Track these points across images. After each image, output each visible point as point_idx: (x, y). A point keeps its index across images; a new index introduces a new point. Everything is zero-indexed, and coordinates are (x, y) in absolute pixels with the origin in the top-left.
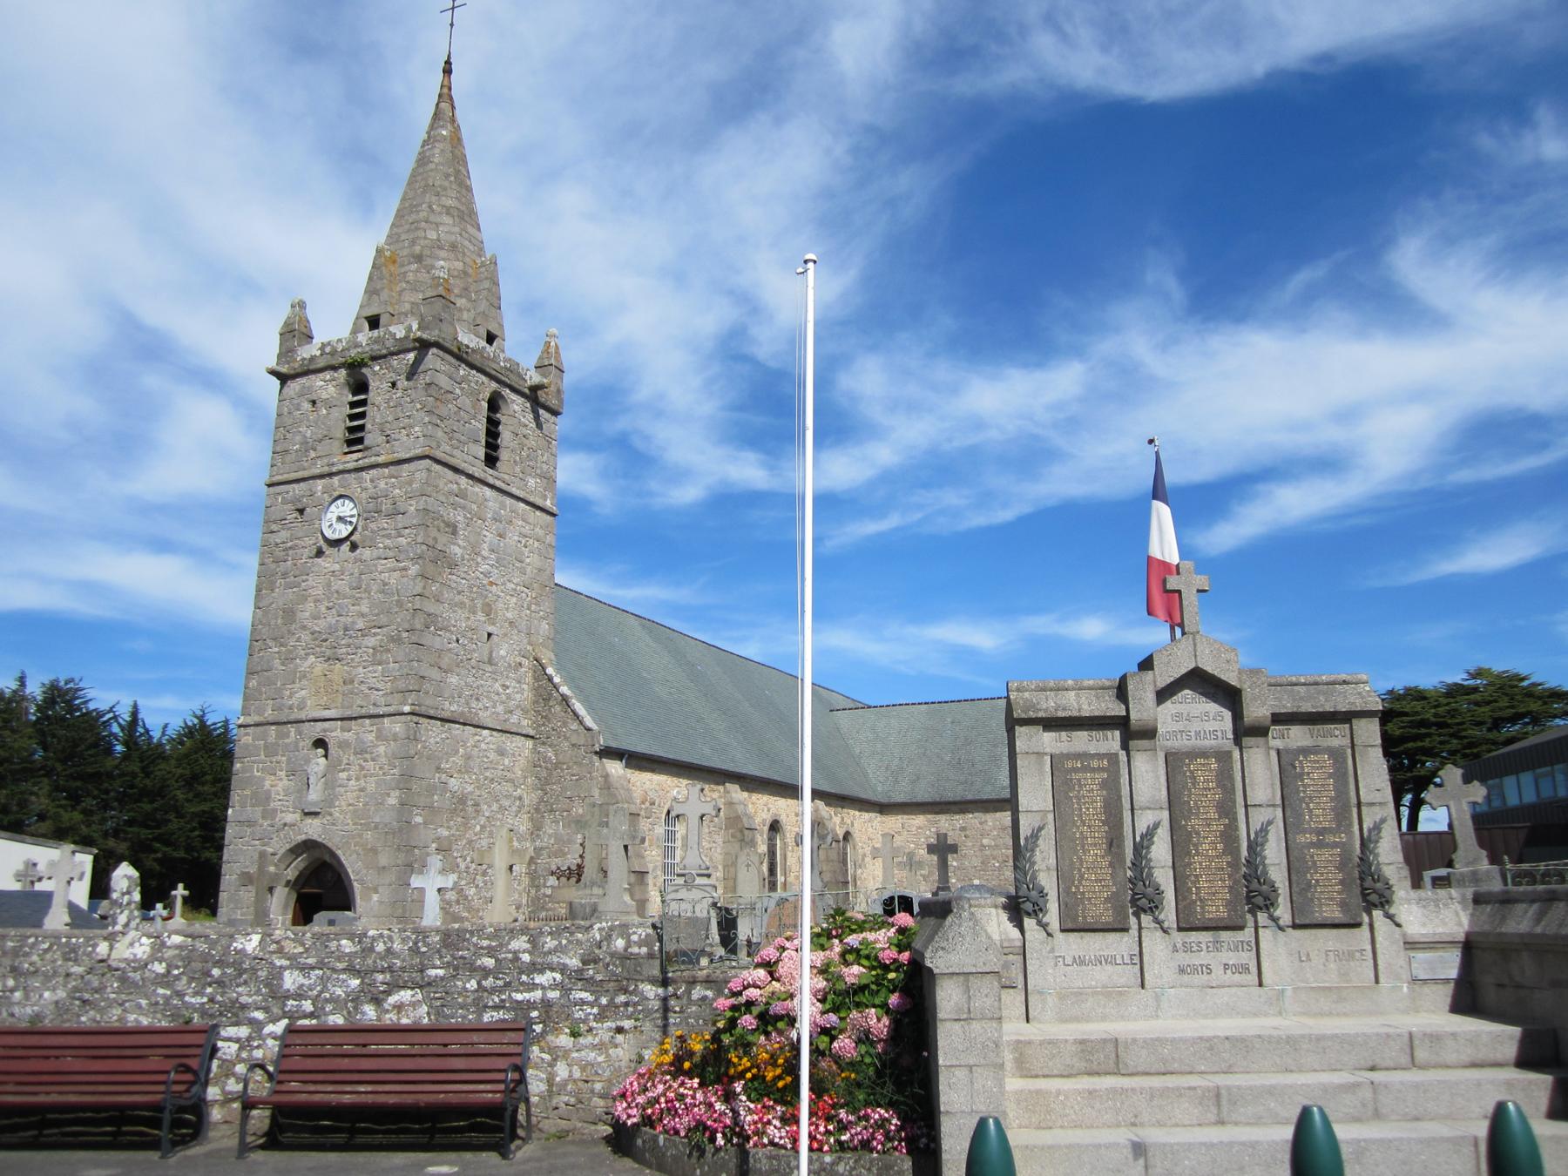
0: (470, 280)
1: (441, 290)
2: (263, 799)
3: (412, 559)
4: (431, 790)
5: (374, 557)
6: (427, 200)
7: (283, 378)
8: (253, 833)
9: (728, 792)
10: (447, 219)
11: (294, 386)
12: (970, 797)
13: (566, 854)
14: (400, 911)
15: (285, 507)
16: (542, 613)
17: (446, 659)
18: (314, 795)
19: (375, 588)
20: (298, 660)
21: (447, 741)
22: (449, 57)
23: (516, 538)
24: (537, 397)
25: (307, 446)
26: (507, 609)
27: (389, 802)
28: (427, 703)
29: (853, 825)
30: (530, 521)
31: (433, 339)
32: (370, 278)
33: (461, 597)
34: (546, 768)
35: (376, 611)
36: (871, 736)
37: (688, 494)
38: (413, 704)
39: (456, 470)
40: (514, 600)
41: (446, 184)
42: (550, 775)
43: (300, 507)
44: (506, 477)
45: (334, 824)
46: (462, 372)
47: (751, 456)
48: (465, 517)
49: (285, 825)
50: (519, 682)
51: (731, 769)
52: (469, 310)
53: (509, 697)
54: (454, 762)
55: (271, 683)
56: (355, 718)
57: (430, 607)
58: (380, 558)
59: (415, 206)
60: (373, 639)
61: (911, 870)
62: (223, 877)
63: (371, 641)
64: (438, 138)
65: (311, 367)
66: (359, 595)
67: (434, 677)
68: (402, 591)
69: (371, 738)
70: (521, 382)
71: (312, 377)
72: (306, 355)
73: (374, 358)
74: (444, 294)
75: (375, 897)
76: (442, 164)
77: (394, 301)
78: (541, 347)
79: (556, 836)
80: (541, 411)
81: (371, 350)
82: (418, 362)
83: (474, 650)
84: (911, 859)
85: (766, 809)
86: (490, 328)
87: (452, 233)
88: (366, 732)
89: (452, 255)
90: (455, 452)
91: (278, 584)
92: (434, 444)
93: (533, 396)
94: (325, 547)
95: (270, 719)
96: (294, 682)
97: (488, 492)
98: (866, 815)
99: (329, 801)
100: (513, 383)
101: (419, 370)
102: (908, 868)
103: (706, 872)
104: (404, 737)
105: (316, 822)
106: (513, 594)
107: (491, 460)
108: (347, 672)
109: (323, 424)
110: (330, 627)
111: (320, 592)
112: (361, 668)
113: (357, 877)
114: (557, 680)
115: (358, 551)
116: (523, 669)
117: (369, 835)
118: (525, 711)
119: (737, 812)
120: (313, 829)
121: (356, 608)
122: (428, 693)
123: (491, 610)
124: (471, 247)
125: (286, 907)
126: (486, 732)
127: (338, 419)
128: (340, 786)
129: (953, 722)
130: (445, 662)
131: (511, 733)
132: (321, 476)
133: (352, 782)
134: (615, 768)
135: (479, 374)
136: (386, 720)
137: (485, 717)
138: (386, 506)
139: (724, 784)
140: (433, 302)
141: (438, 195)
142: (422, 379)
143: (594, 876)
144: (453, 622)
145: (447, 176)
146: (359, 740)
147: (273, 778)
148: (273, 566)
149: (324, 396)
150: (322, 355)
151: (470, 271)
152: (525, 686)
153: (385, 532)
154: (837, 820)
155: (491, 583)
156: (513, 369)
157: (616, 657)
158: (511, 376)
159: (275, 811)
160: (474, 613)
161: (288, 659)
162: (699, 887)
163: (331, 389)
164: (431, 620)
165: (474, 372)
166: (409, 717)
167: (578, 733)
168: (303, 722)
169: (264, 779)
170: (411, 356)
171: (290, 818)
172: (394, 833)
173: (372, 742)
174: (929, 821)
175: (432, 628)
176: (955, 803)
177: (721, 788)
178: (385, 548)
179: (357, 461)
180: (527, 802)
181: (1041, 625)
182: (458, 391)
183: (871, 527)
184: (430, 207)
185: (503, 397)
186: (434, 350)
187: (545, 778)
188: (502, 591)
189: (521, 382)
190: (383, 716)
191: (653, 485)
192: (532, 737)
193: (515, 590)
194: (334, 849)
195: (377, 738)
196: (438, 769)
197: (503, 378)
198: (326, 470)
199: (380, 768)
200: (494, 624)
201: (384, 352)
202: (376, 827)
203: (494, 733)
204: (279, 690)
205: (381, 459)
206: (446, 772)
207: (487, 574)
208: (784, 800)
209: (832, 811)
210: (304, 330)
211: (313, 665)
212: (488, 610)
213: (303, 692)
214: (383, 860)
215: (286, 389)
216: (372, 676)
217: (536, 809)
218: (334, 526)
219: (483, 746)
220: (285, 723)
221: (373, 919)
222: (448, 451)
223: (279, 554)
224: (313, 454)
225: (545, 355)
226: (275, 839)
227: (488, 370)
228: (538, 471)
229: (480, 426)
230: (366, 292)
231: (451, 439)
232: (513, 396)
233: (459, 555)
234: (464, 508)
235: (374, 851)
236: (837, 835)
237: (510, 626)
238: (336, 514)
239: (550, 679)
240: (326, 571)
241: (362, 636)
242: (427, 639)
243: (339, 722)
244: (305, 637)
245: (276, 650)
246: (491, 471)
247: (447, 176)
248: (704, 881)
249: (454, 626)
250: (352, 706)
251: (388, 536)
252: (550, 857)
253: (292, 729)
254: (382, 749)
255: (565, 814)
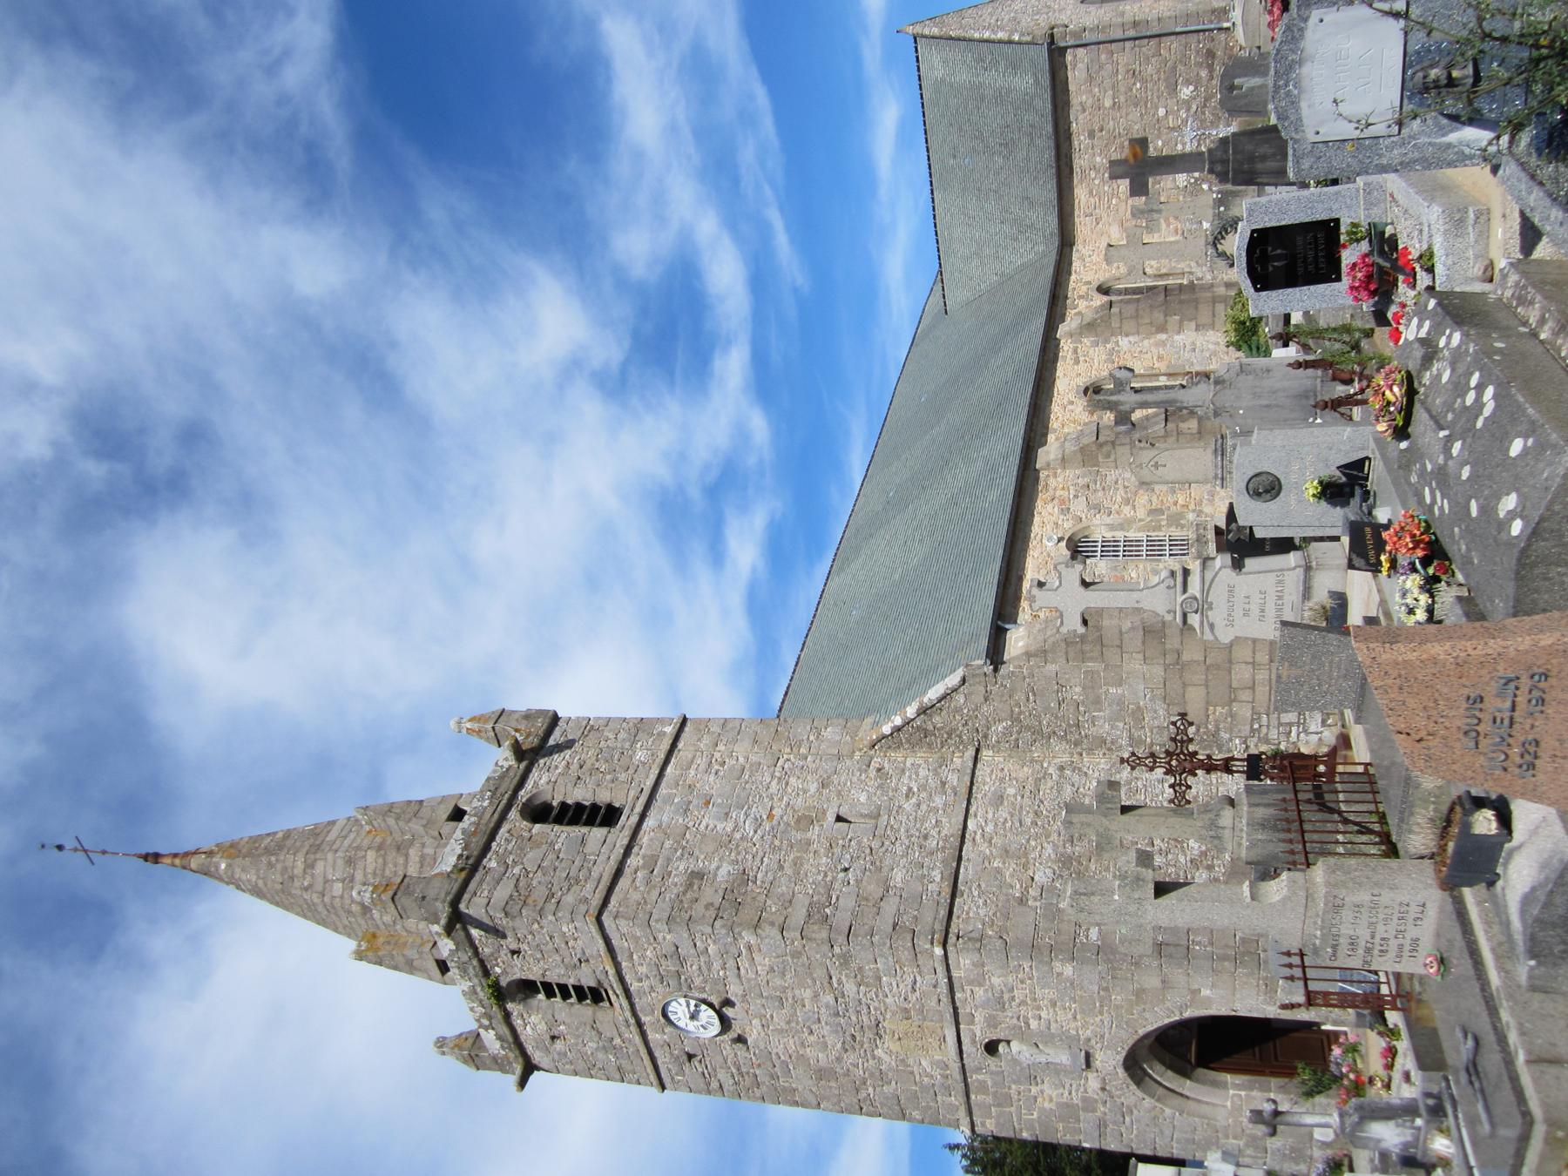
0: (389, 841)
1: (387, 897)
2: (1069, 1112)
3: (735, 939)
4: (1054, 913)
5: (738, 981)
6: (298, 892)
7: (529, 1068)
8: (1115, 1123)
9: (1048, 464)
10: (320, 867)
11: (537, 1057)
12: (1050, 128)
13: (1139, 708)
14: (1226, 963)
15: (687, 1071)
16: (812, 738)
17: (872, 887)
18: (1063, 1058)
19: (778, 982)
20: (883, 1067)
21: (983, 886)
22: (135, 855)
23: (712, 778)
24: (532, 750)
25: (609, 1047)
26: (805, 792)
27: (1071, 973)
28: (930, 920)
29: (1089, 283)
30: (690, 756)
31: (447, 909)
32: (395, 968)
33: (786, 865)
34: (1019, 732)
35: (809, 981)
36: (975, 262)
37: (759, 425)
38: (932, 943)
39: (618, 873)
40: (793, 780)
41: (279, 866)
42: (1028, 728)
43: (685, 1058)
44: (632, 793)
45: (1102, 1037)
46: (493, 864)
47: (717, 363)
48: (680, 859)
49: (1103, 1089)
50: (903, 771)
51: (1017, 461)
52: (423, 845)
53: (923, 788)
54: (1012, 876)
55: (915, 1095)
56: (955, 1009)
57: (798, 914)
58: (739, 975)
59: (309, 907)
60: (846, 986)
61: (1159, 211)
62: (1175, 1156)
63: (850, 988)
64: (230, 874)
65: (511, 1039)
66: (790, 1000)
67: (895, 907)
68: (779, 952)
69: (982, 992)
70: (511, 774)
71: (523, 1038)
72: (498, 1045)
73: (486, 973)
74: (390, 893)
75: (1206, 992)
76: (258, 870)
77: (419, 941)
78: (475, 739)
79: (1112, 720)
80: (551, 742)
81: (476, 976)
82: (480, 925)
83: (859, 843)
84: (1142, 212)
85: (1070, 407)
86: (445, 816)
87: (335, 862)
88: (973, 999)
89: (360, 864)
90: (595, 874)
91: (786, 1085)
92: (583, 908)
93: (528, 756)
94: (732, 1034)
95: (962, 1099)
96: (912, 1073)
97: (649, 823)
98: (1076, 265)
99: (1070, 1041)
100: (512, 787)
101: (491, 924)
102: (1155, 216)
103: (1179, 579)
104: (978, 955)
105: (1099, 1059)
106: (784, 781)
107: (607, 816)
108: (894, 1014)
109: (577, 1029)
110: (837, 1032)
111: (791, 1042)
112: (887, 1000)
113: (1177, 1013)
114: (898, 721)
115: (733, 999)
116: (886, 765)
117: (1117, 998)
118: (943, 762)
119: (1074, 452)
120: (1110, 1060)
121: (807, 1002)
122: (916, 918)
123: (805, 817)
124: (352, 836)
125: (1215, 1084)
126: (971, 824)
127: (569, 1013)
128: (1049, 1029)
129: (955, 157)
130: (874, 890)
131: (972, 783)
132: (643, 1034)
133: (1044, 1014)
134: (1017, 640)
135: (497, 838)
136: (955, 974)
137: (951, 826)
138: (670, 966)
139: (1037, 471)
140: (403, 907)
141: (292, 878)
142: (501, 921)
143: (1199, 824)
144: (820, 878)
145: (270, 865)
146: (985, 1005)
147: (1040, 1100)
148: (764, 1089)
149: (542, 1027)
150: (493, 1029)
151: (378, 839)
152: (909, 762)
153: (704, 968)
154: (1082, 305)
155: (770, 816)
156: (493, 785)
157: (874, 617)
158: (502, 790)
159: (1084, 1100)
160: (809, 843)
161: (882, 1077)
162: (1206, 590)
163: (534, 1019)
164: (818, 914)
165: (494, 845)
166: (950, 948)
167: (971, 693)
168: (963, 1066)
169: (1042, 1110)
170: (475, 932)
171: (1093, 1083)
172: (1114, 969)
173: (986, 990)
174: (1081, 181)
175: (827, 910)
176: (1058, 147)
177: (1042, 475)
178: (724, 968)
179: (617, 996)
180: (1066, 758)
181: (872, 54)
182: (516, 870)
183: (782, 239)
184: (306, 889)
185: (529, 800)
186: (462, 907)
187: (1033, 734)
188: (781, 800)
189: (511, 774)
190: (950, 978)
191: (752, 461)
192: (978, 751)
193: (780, 778)
194: (1136, 1037)
195: (980, 985)
196: (1022, 901)
197: (504, 801)
198: (634, 1028)
199: (1022, 982)
200: (824, 813)
201: (475, 962)
202: (1106, 989)
203: (972, 811)
204: (924, 1088)
205: (612, 972)
206: (1026, 889)
207: (758, 823)
208: (1057, 381)
209: (1070, 313)
210: (471, 1041)
211: (887, 1052)
212: (806, 821)
213: (924, 1063)
214: (1152, 982)
215: (542, 1065)
216: (895, 989)
217: (1076, 745)
218: (703, 1023)
219: (989, 828)
220: (966, 1085)
221: (1238, 996)
222: (593, 886)
223: (748, 1081)
224: (617, 1041)
225: (483, 734)
226: (1123, 1099)
227: (492, 825)
228: (627, 745)
229: (564, 836)
230: (412, 973)
231: (577, 882)
232: (529, 785)
233: (731, 868)
234: (669, 860)
235: (1140, 993)
236: (1102, 305)
237: (828, 785)
238: (688, 1021)
239: (898, 729)
240: (763, 1034)
241: (843, 996)
242: (842, 919)
243: (962, 1026)
244: (850, 1058)
245: (871, 1090)
246: (623, 818)
247: (270, 865)
248: (1195, 580)
249: (826, 875)
250: (940, 1011)
251: (709, 965)
252: (1143, 727)
253: (973, 1078)
254: (996, 981)
255: (1081, 709)
